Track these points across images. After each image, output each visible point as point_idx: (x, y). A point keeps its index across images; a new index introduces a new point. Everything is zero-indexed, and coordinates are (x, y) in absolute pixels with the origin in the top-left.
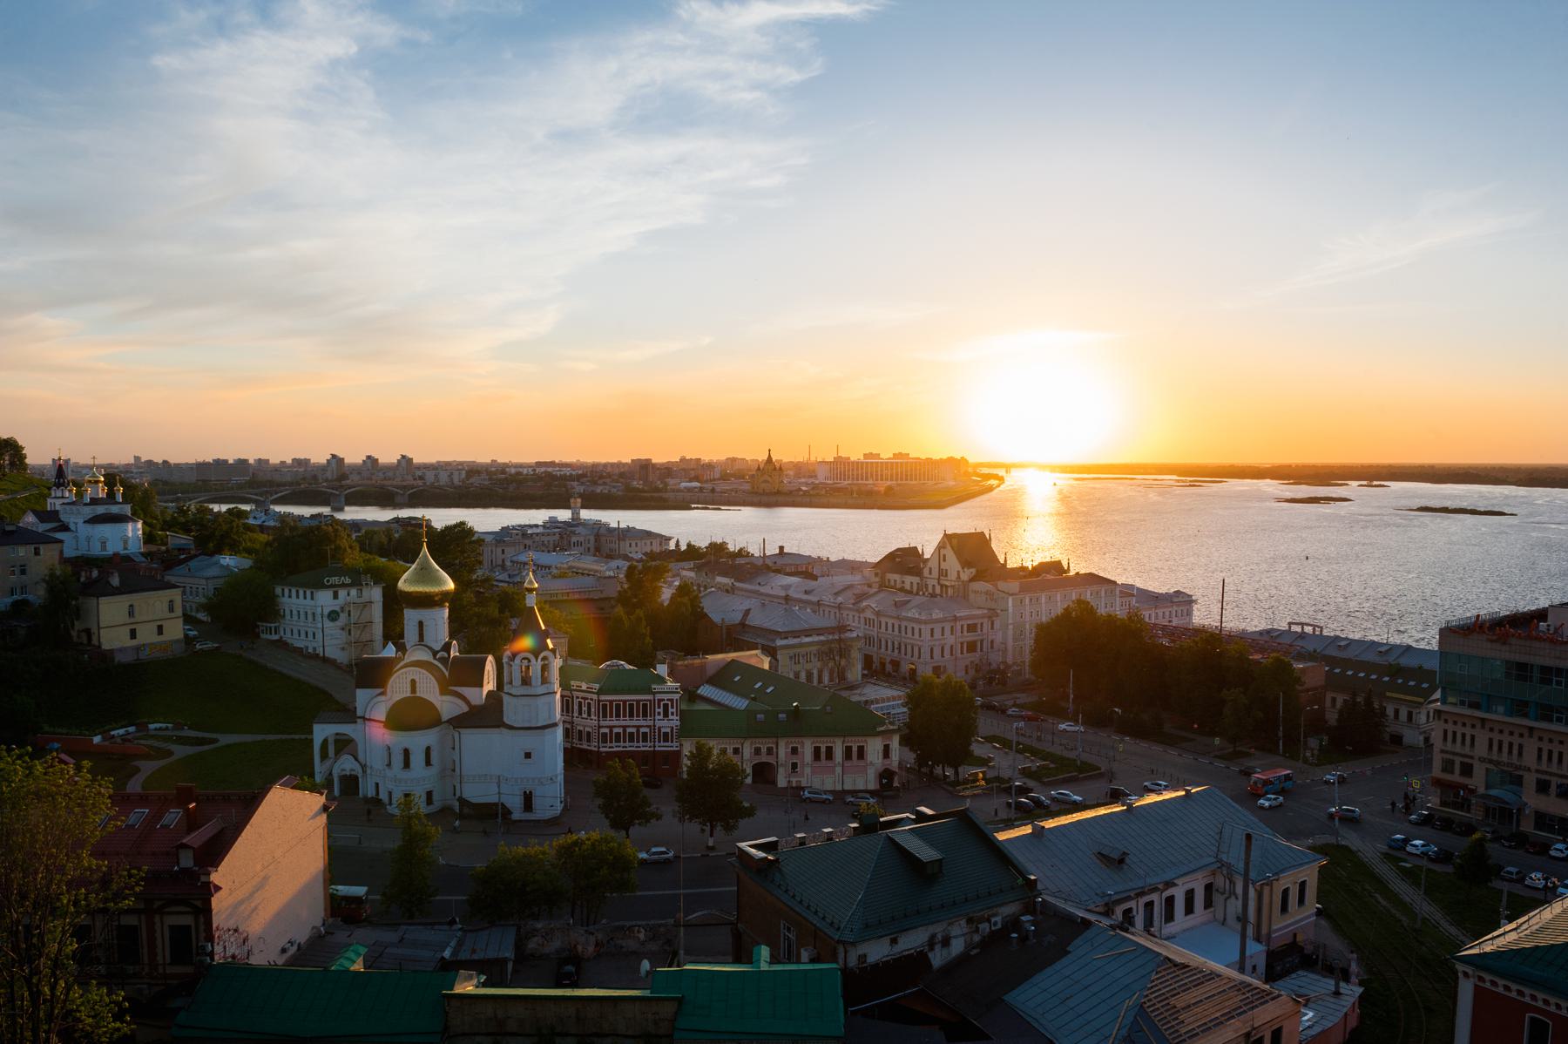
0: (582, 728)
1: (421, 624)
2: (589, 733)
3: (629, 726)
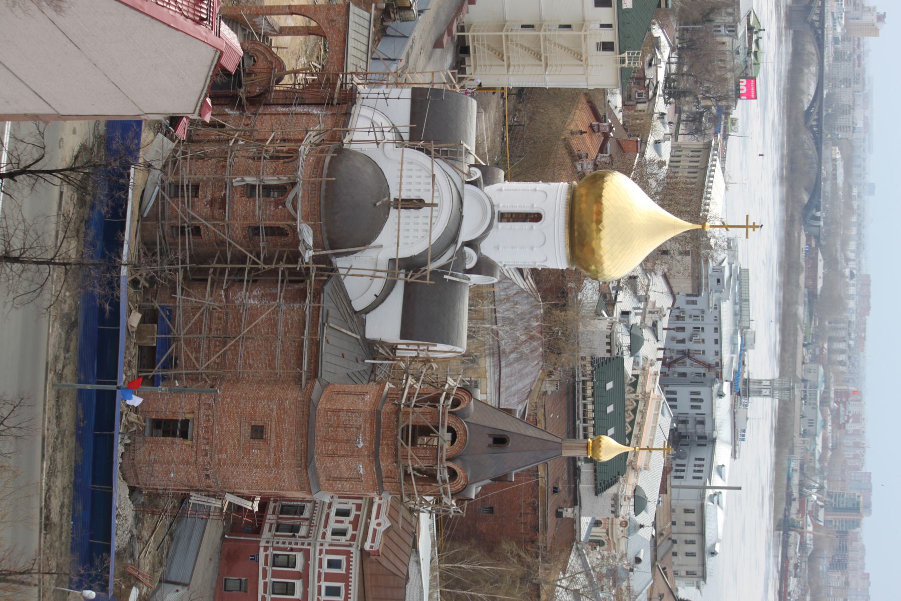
0: (306, 514)
1: (536, 217)
2: (294, 529)
3: (306, 585)
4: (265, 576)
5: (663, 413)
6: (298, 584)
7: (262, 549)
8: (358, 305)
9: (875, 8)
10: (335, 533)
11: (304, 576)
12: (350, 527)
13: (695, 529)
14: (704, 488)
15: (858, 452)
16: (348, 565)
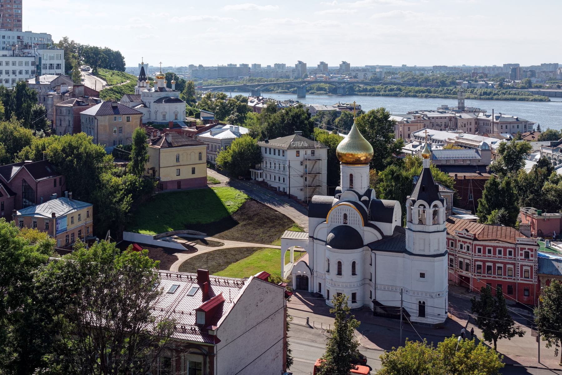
0: (462, 260)
1: (351, 176)
3: (498, 262)
4: (495, 278)
5: (463, 136)
6: (508, 266)
7: (475, 277)
8: (380, 237)
9: (296, 65)
10: (468, 249)
11: (484, 262)
12: (466, 244)
13: (508, 126)
14: (493, 122)
15: (496, 69)
16: (510, 248)
